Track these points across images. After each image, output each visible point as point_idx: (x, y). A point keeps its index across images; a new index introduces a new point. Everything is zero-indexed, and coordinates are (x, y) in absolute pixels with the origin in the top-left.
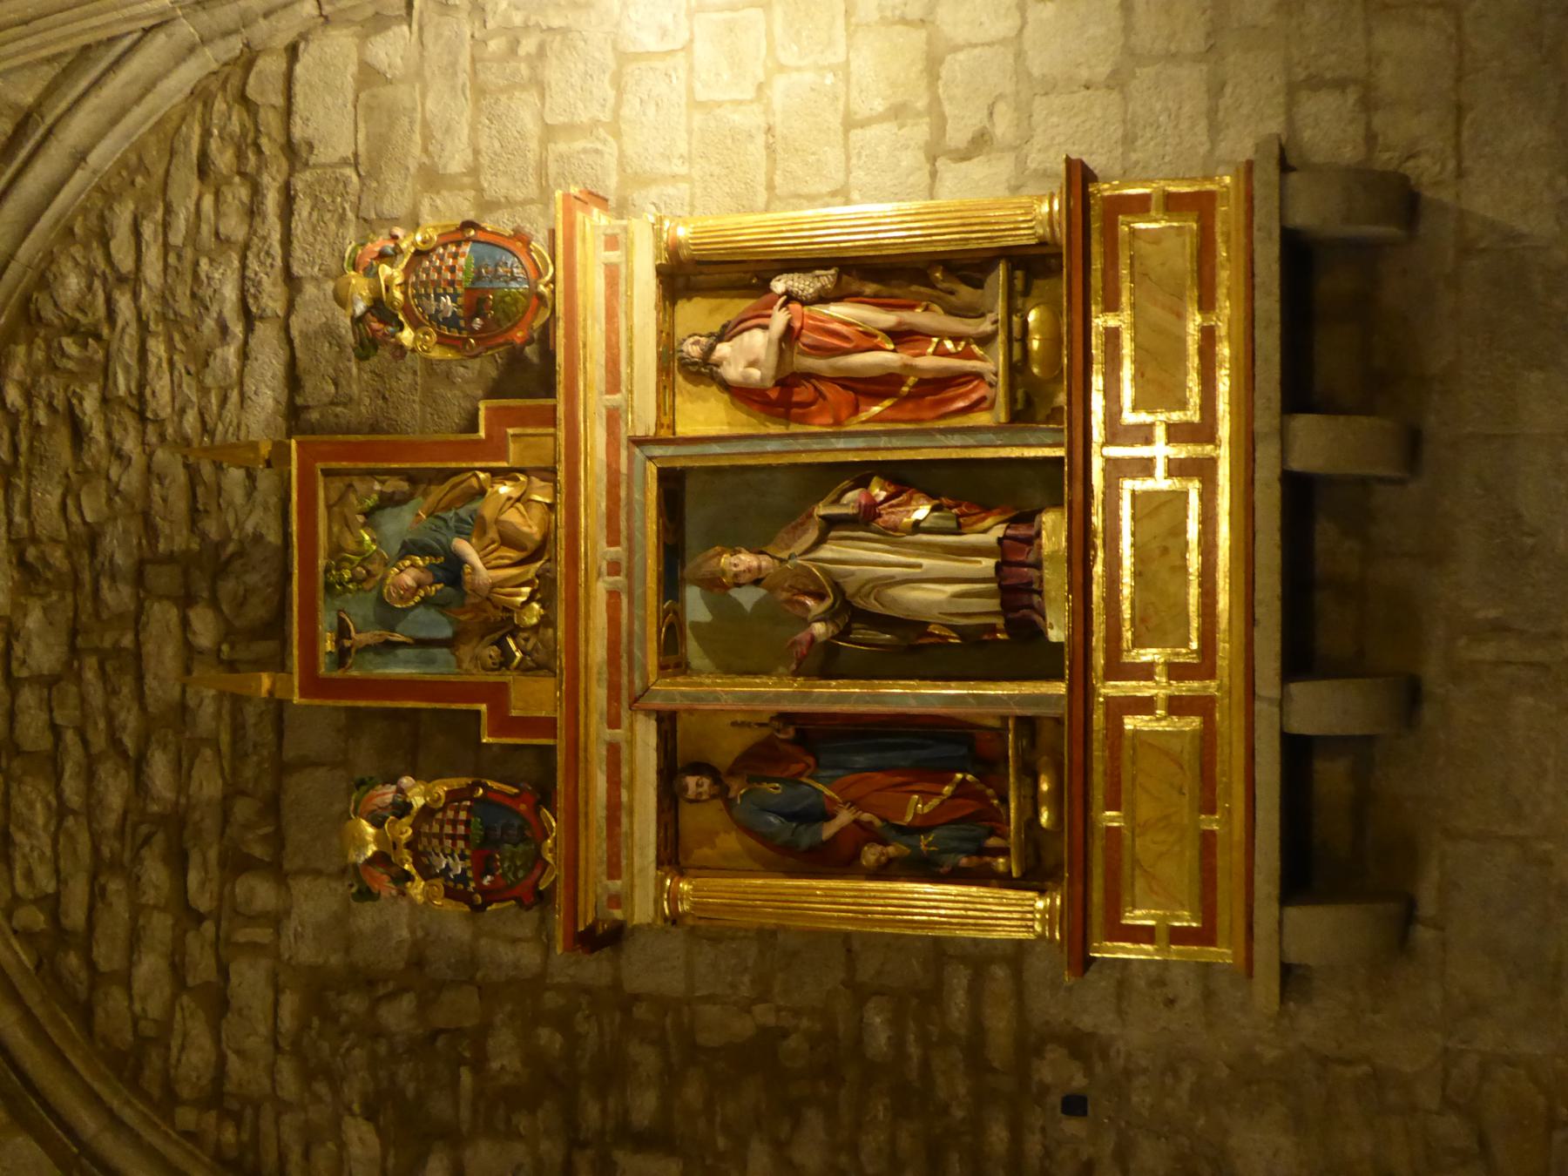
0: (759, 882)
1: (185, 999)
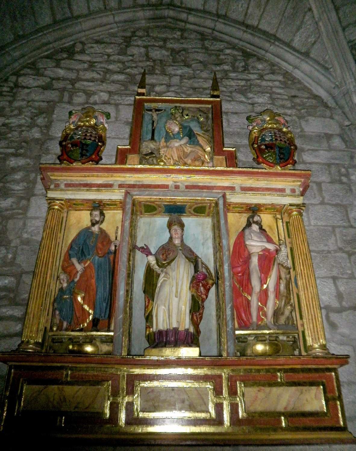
0: (108, 286)
1: (49, 80)
